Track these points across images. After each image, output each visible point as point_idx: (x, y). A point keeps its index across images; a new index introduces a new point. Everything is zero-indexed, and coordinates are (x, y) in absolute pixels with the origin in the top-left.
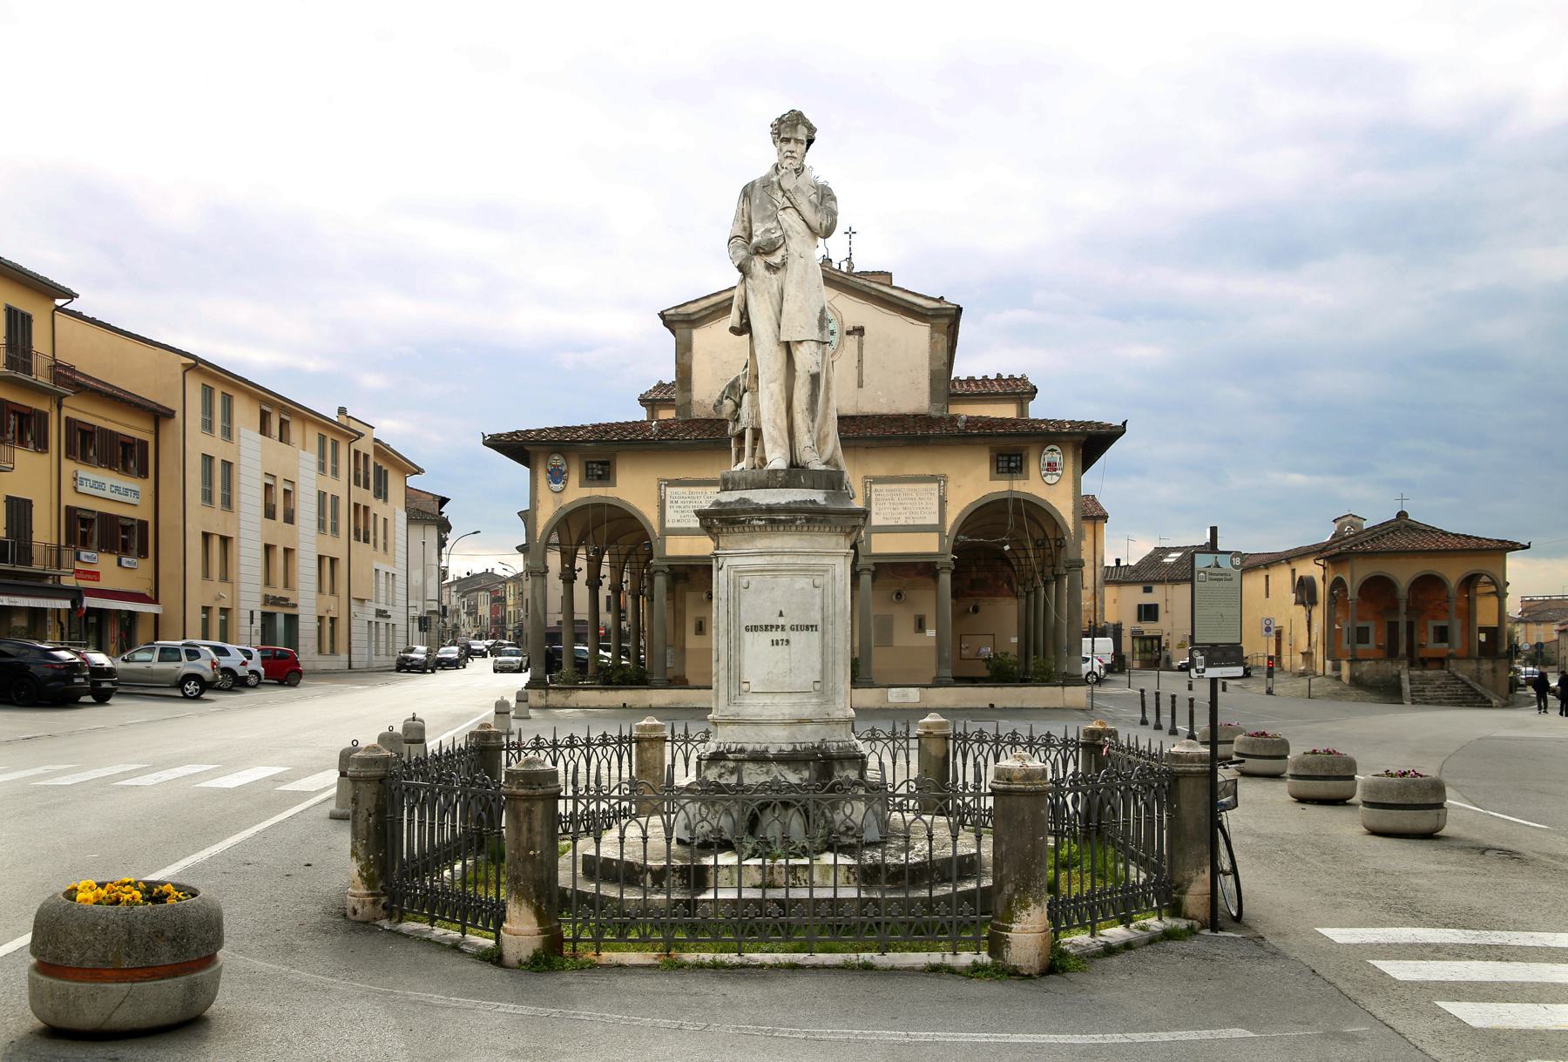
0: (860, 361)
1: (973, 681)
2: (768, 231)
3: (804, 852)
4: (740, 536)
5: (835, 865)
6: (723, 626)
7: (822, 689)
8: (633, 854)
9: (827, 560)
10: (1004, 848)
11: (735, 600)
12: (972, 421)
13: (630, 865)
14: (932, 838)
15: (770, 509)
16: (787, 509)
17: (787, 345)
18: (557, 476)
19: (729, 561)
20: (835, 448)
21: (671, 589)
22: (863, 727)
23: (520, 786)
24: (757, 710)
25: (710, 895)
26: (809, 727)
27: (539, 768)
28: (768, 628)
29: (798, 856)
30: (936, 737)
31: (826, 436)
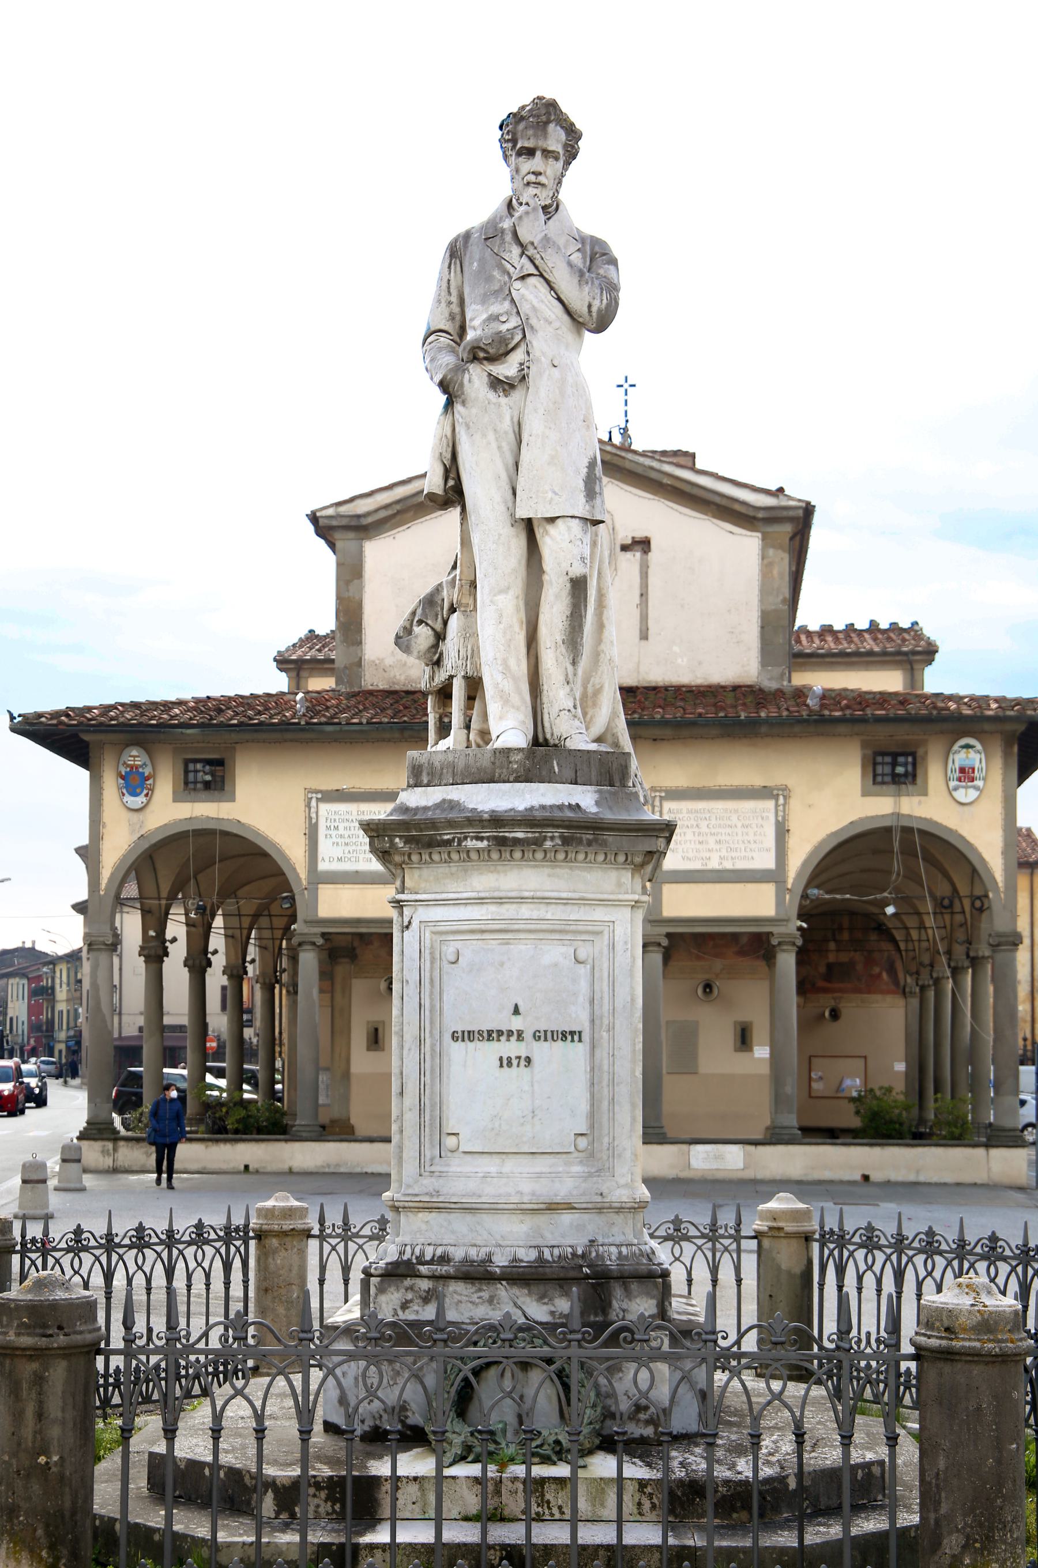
0: (644, 595)
1: (831, 1135)
2: (495, 318)
3: (558, 1453)
4: (443, 869)
5: (620, 1479)
6: (411, 1032)
7: (592, 1147)
8: (237, 1453)
9: (599, 914)
10: (942, 1464)
11: (432, 984)
12: (830, 697)
13: (234, 1474)
14: (791, 1431)
15: (497, 820)
16: (529, 820)
17: (529, 525)
18: (135, 783)
19: (422, 914)
20: (614, 715)
21: (326, 975)
22: (662, 1215)
23: (24, 1329)
24: (472, 1185)
25: (381, 1536)
26: (566, 1218)
27: (60, 1295)
28: (491, 1035)
29: (546, 1460)
30: (789, 1236)
31: (597, 692)
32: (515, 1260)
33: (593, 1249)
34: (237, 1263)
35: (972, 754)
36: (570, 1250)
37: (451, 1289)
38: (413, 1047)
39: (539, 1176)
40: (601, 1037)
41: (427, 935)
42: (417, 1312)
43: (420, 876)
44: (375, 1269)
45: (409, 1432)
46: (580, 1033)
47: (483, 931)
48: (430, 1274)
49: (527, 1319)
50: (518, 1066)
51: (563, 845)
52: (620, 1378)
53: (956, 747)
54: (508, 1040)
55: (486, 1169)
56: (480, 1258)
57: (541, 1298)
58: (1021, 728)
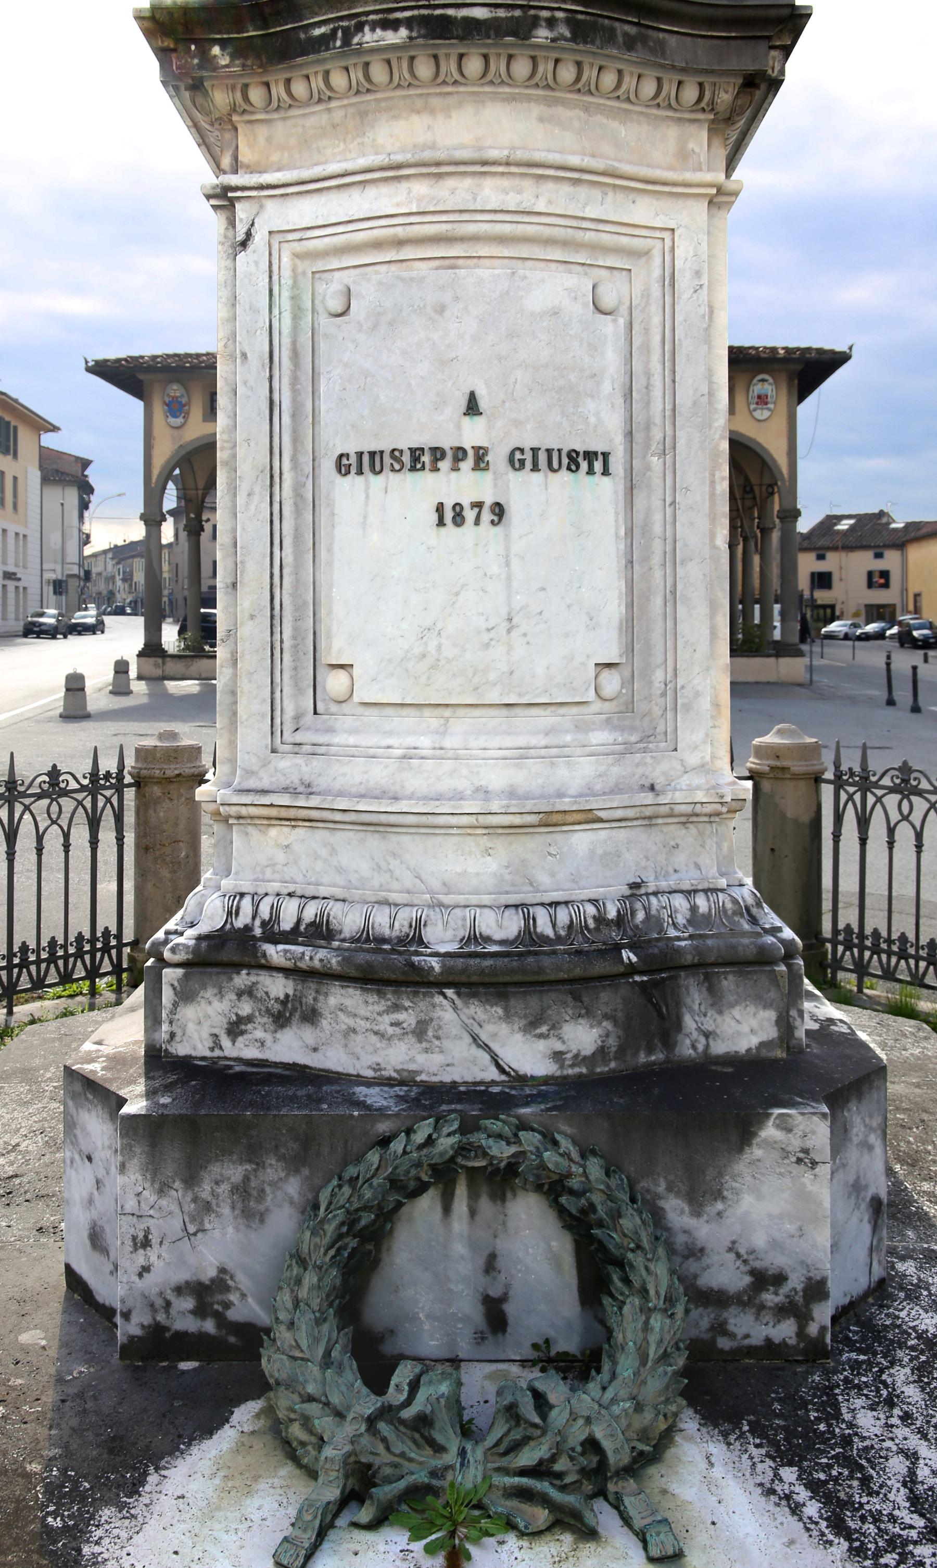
4: (316, 118)
7: (633, 698)
9: (643, 211)
18: (176, 408)
19: (277, 215)
24: (379, 774)
26: (582, 841)
28: (417, 459)
30: (796, 777)
32: (474, 938)
33: (638, 905)
34: (108, 820)
35: (766, 386)
36: (591, 910)
37: (333, 1001)
38: (257, 489)
39: (523, 754)
40: (648, 468)
41: (285, 259)
42: (263, 1044)
43: (269, 139)
44: (173, 950)
45: (232, 1339)
46: (606, 455)
47: (400, 243)
48: (289, 964)
49: (502, 1071)
50: (477, 522)
51: (574, 39)
52: (719, 1214)
53: (755, 381)
54: (455, 469)
55: (410, 741)
56: (395, 933)
57: (533, 1024)
58: (799, 367)
